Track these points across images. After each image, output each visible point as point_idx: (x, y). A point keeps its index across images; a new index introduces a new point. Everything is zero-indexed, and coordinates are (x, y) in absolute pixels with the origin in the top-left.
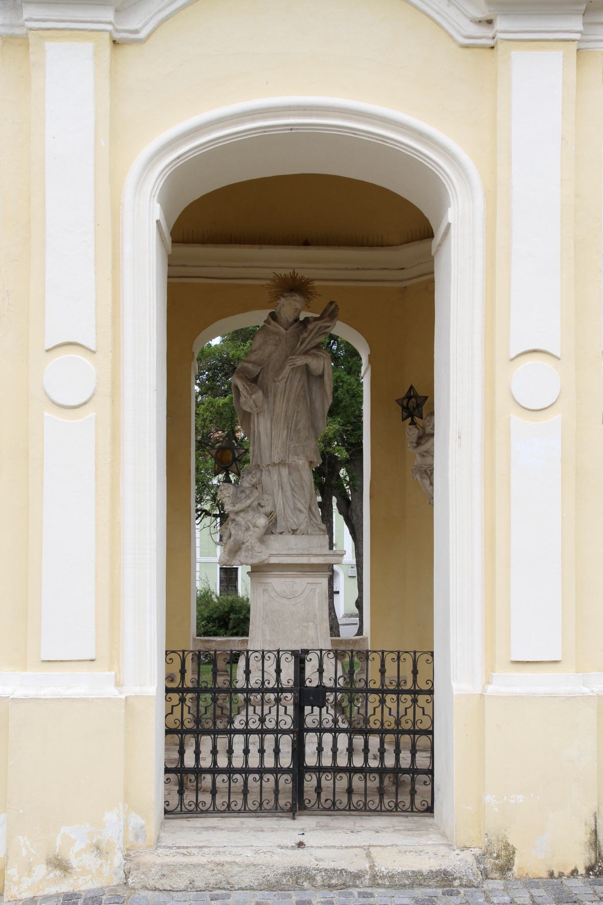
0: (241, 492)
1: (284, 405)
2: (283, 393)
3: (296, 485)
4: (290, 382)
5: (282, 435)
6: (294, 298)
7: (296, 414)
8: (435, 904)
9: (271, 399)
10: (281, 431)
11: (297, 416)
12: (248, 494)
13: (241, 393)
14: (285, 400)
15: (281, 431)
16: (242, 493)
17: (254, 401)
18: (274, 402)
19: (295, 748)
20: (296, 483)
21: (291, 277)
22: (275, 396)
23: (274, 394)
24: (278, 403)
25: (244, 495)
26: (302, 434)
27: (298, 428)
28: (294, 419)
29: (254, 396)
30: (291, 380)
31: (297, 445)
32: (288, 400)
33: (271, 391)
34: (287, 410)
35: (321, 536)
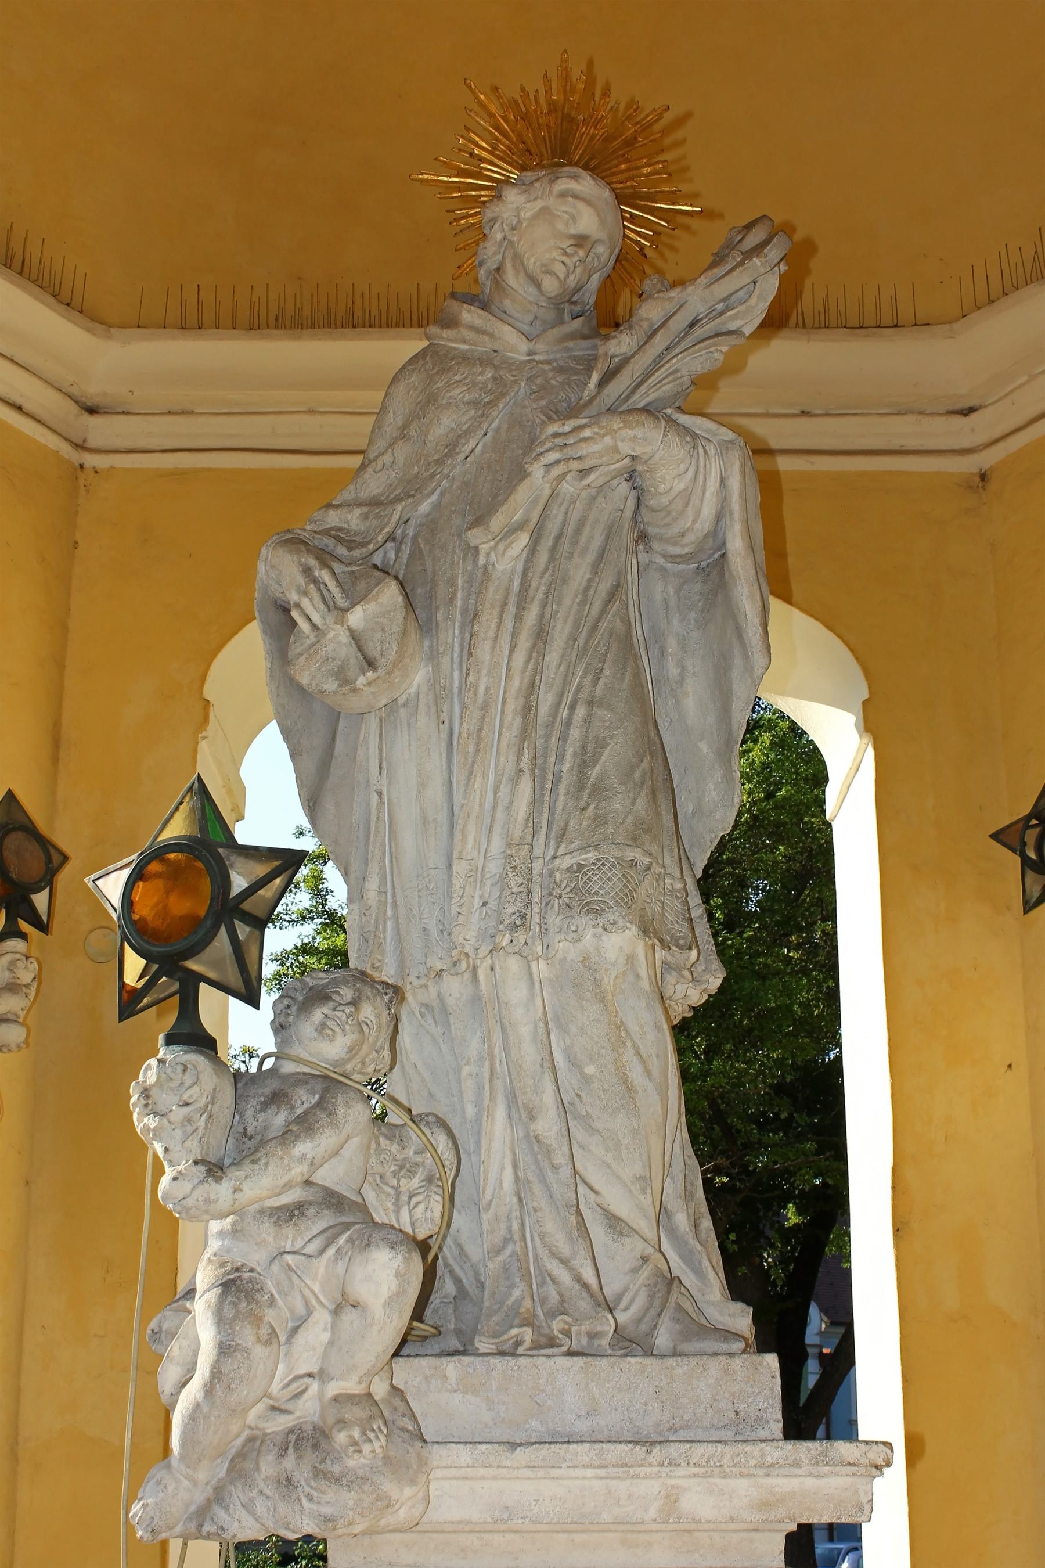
0: (264, 1106)
1: (519, 658)
2: (511, 609)
3: (587, 1080)
4: (552, 558)
5: (509, 808)
6: (564, 184)
7: (581, 711)
8: (833, 1561)
9: (451, 634)
10: (504, 790)
11: (588, 721)
12: (306, 1113)
13: (295, 614)
14: (524, 642)
15: (504, 790)
16: (273, 1108)
17: (354, 635)
18: (469, 650)
19: (835, 1004)
20: (590, 1070)
21: (553, 107)
22: (471, 618)
23: (465, 612)
24: (484, 651)
25: (279, 1119)
26: (618, 805)
27: (594, 773)
28: (575, 733)
29: (356, 618)
30: (553, 550)
31: (591, 856)
32: (541, 635)
33: (452, 599)
34: (532, 685)
35: (737, 1362)
